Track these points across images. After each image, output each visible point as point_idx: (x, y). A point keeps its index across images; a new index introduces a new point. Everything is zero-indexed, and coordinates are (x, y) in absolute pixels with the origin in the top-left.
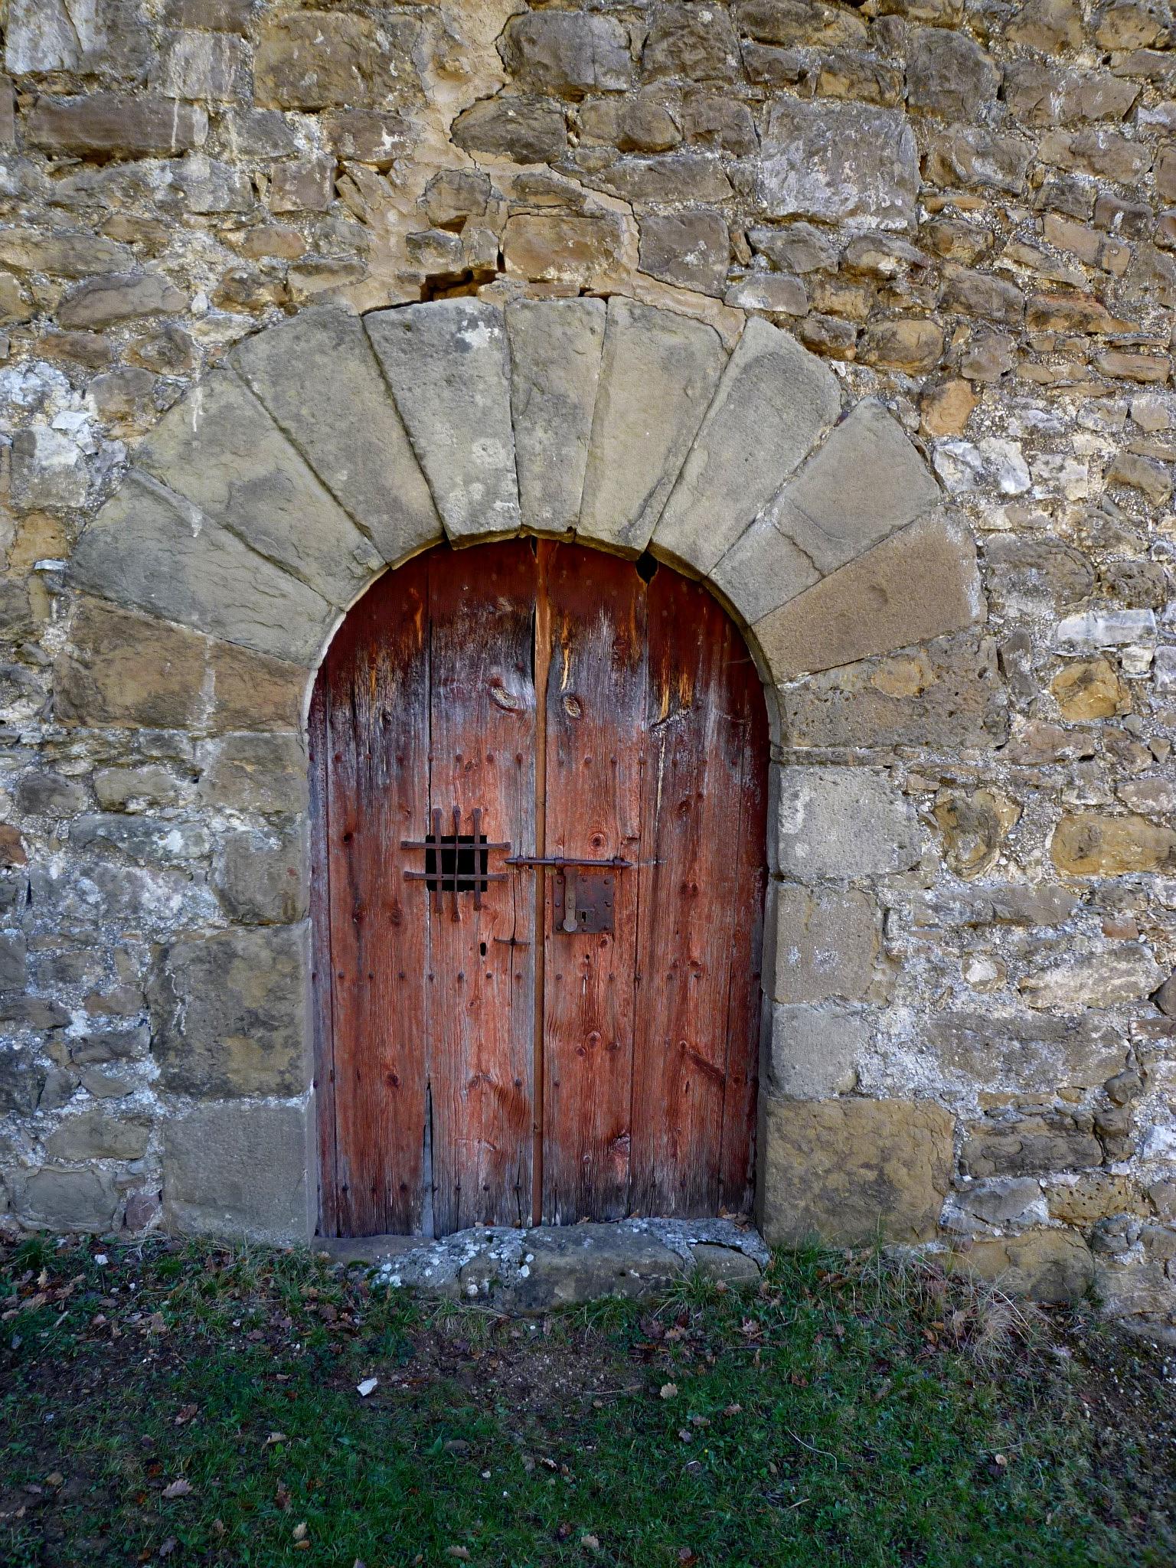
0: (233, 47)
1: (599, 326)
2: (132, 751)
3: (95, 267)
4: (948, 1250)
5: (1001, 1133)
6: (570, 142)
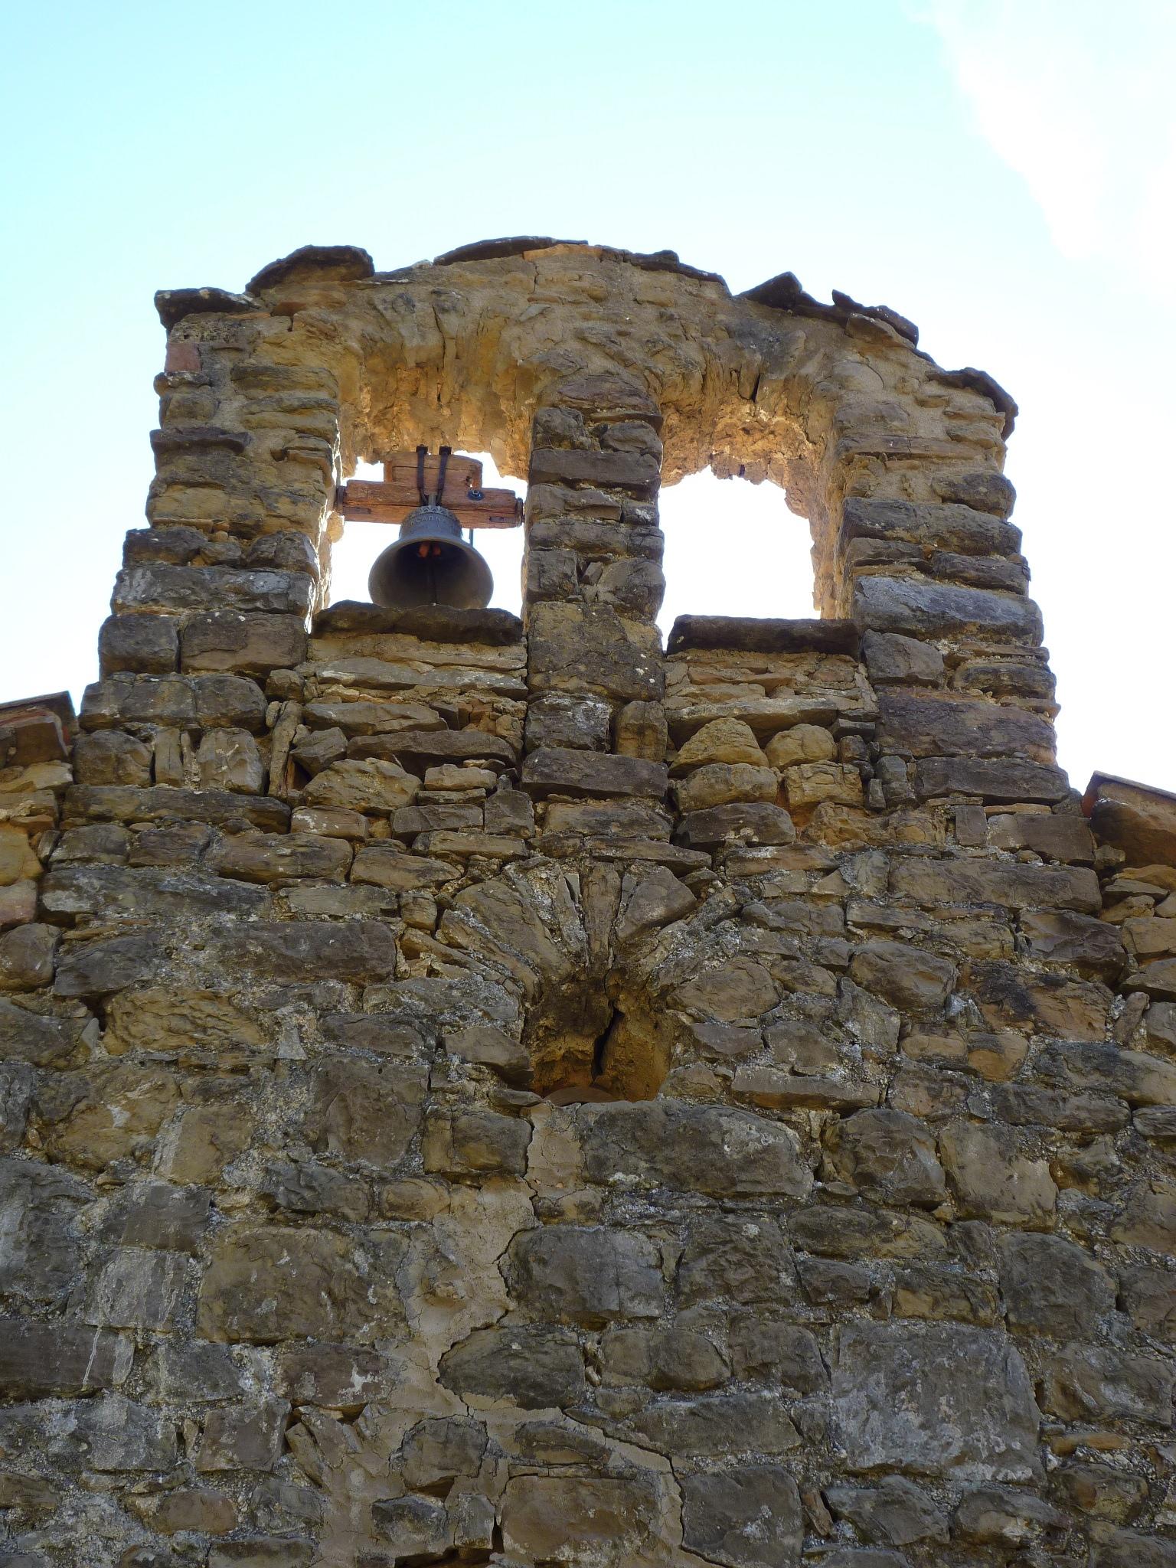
0: (179, 1268)
6: (588, 1378)
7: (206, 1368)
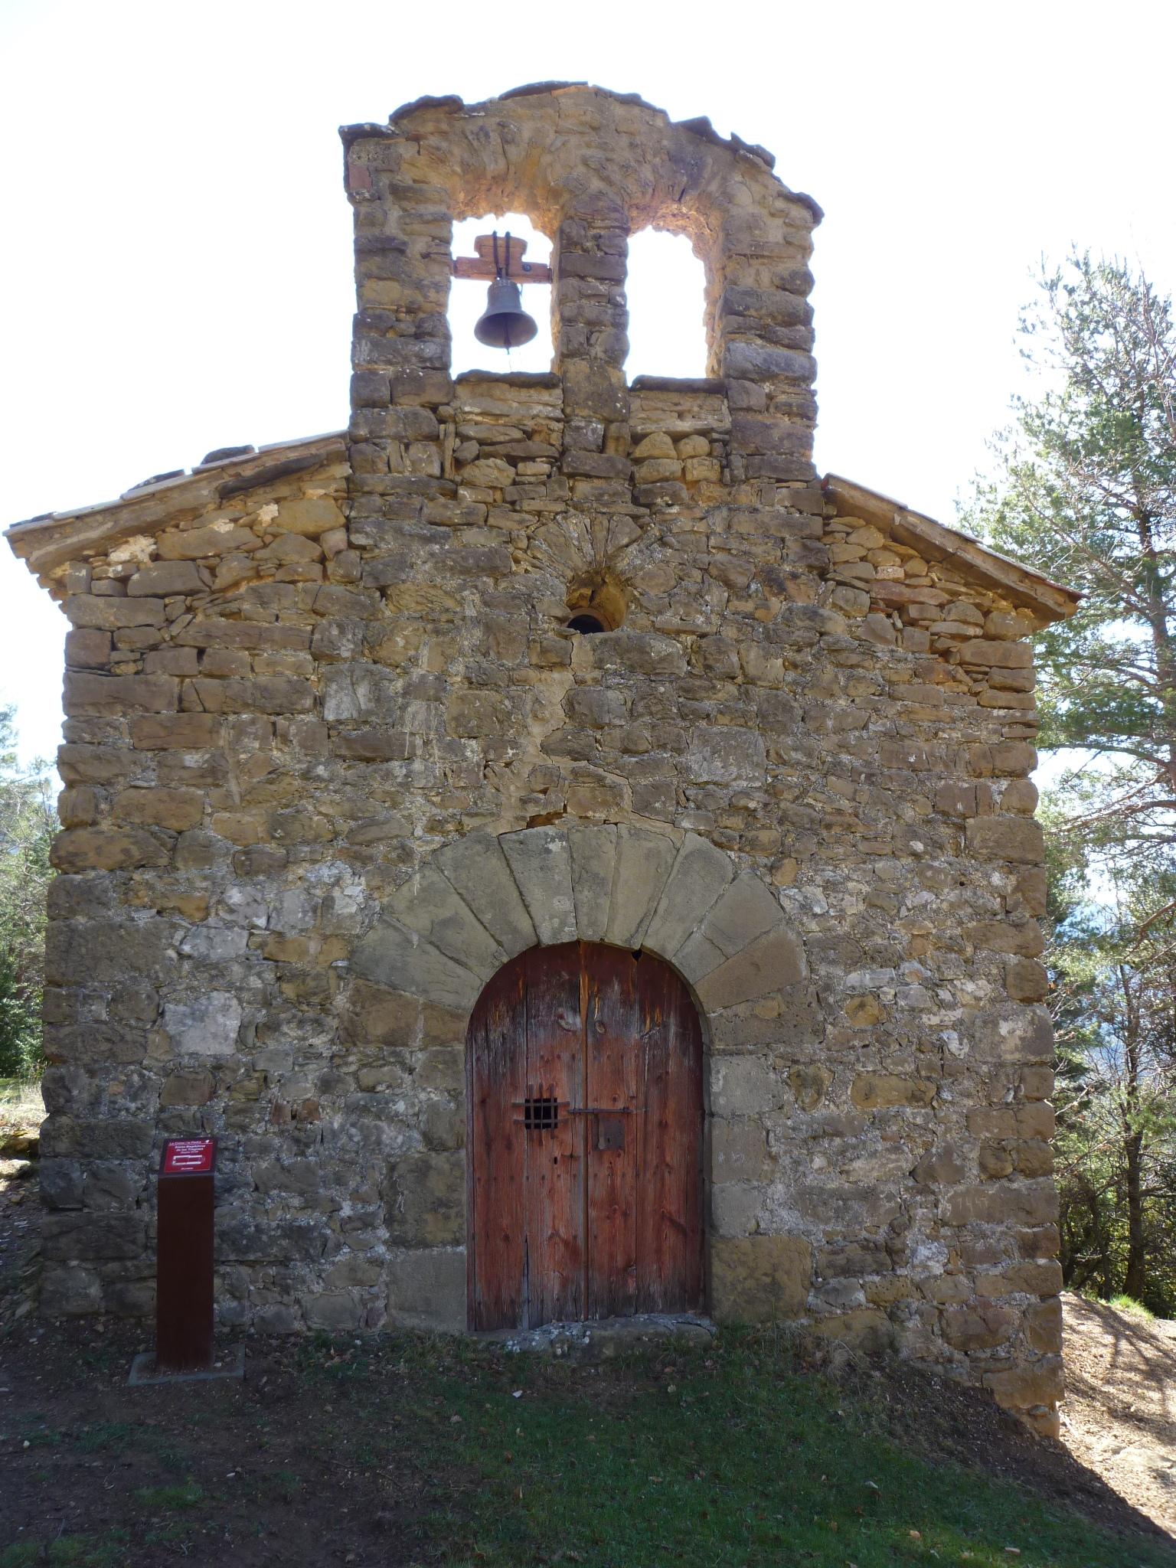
1: (614, 839)
2: (379, 1059)
3: (367, 815)
4: (813, 1322)
5: (834, 1253)
7: (452, 748)
